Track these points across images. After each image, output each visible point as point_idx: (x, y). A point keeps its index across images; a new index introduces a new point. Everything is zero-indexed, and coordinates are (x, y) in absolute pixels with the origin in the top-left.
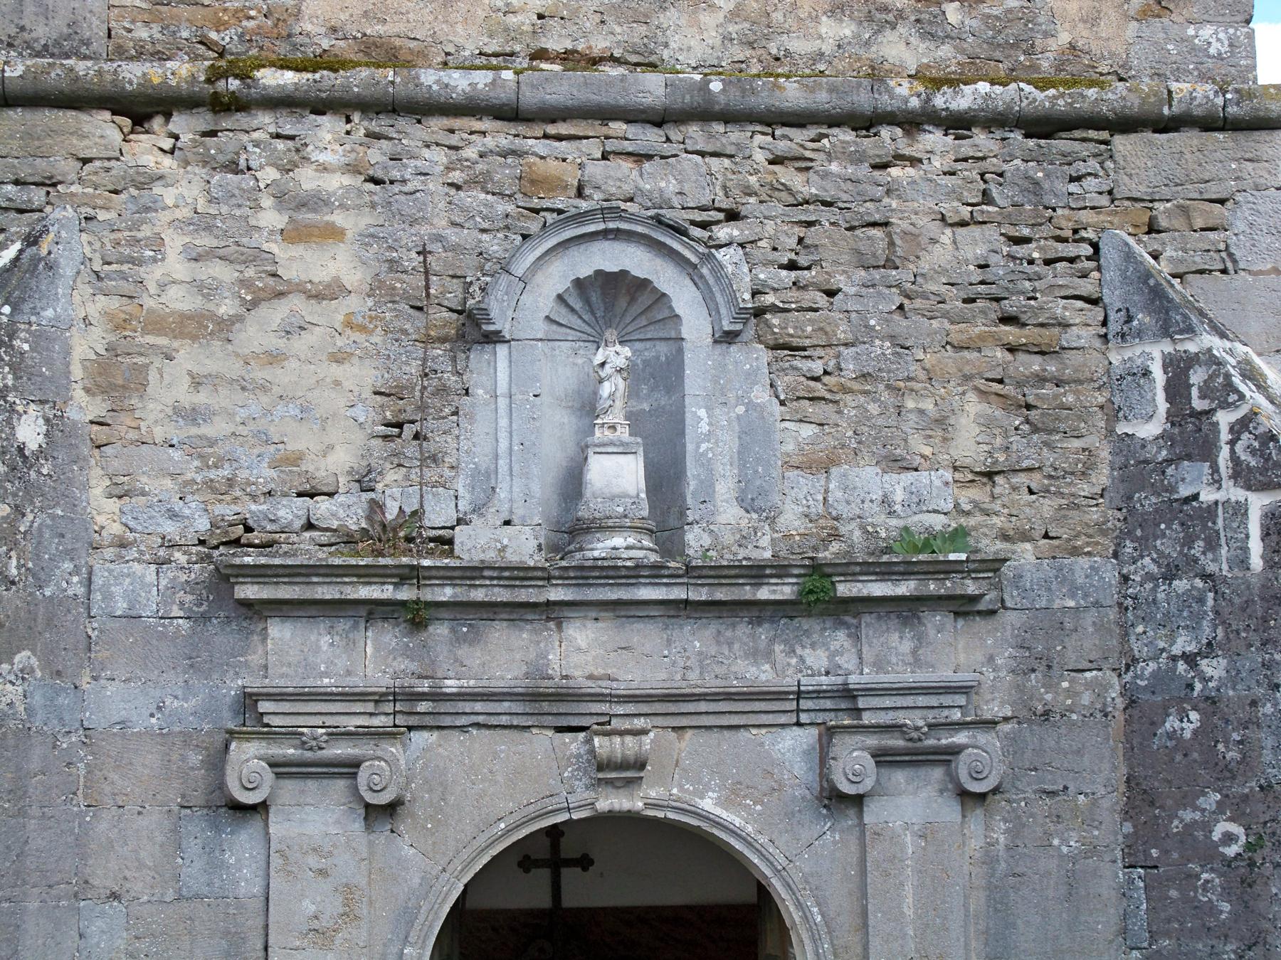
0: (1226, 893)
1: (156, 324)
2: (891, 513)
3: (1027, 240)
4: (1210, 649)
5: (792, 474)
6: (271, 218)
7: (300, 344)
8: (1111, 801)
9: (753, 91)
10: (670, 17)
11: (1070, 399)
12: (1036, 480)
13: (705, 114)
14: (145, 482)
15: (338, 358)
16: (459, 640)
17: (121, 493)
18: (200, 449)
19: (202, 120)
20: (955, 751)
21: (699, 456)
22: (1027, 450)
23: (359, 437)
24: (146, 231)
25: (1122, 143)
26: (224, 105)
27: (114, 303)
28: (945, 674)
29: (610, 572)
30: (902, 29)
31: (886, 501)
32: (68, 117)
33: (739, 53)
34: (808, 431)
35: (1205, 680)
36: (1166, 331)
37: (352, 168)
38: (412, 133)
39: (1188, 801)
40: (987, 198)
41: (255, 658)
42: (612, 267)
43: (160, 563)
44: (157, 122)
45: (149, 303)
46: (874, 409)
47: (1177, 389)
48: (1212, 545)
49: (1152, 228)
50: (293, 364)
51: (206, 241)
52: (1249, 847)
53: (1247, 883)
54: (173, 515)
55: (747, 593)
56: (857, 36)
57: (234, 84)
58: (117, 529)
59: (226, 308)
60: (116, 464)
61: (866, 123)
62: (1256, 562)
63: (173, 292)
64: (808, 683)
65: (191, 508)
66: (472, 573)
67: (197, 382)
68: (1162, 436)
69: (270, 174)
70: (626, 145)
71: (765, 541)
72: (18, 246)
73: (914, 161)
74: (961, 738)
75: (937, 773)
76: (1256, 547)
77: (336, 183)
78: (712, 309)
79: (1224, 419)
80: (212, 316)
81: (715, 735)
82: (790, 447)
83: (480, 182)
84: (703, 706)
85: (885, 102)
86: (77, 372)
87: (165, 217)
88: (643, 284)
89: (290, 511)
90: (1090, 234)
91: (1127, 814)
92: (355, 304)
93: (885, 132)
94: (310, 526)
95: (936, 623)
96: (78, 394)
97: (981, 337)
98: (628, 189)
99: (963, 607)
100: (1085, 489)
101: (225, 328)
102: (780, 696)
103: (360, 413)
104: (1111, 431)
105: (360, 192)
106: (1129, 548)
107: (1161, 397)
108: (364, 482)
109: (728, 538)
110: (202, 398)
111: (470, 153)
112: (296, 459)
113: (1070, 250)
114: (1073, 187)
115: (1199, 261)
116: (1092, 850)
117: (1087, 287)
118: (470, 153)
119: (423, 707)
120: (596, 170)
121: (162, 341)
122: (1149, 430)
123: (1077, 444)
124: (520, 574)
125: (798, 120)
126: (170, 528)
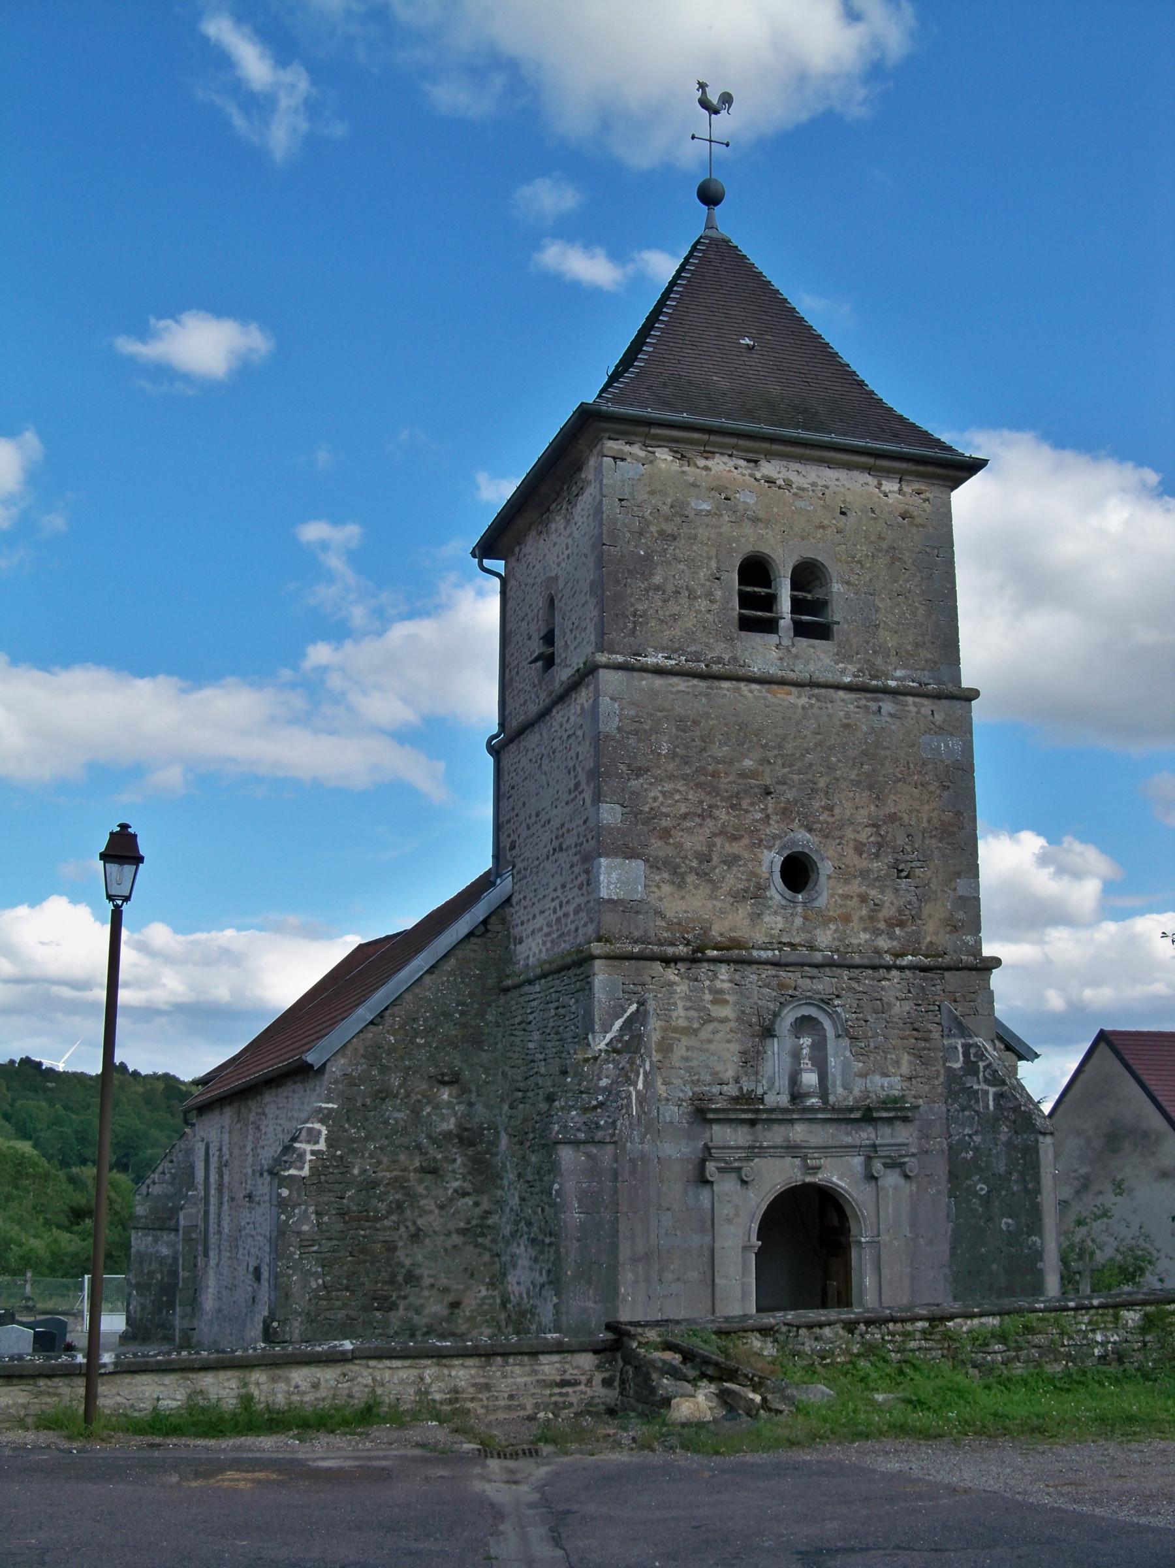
0: (981, 1206)
1: (675, 1030)
2: (884, 1090)
3: (920, 1005)
4: (976, 1133)
5: (857, 1078)
6: (708, 997)
7: (718, 1037)
8: (944, 1178)
9: (846, 959)
10: (817, 932)
11: (932, 1055)
12: (923, 1080)
13: (832, 964)
14: (674, 1081)
15: (729, 1041)
16: (764, 1130)
17: (665, 1083)
18: (689, 1070)
19: (687, 965)
20: (904, 1163)
21: (832, 1073)
22: (921, 1071)
23: (735, 1066)
24: (672, 1001)
25: (947, 974)
26: (694, 961)
27: (663, 1023)
28: (900, 1140)
29: (812, 1109)
30: (883, 936)
31: (882, 1086)
32: (648, 963)
33: (837, 943)
34: (861, 1065)
35: (974, 1142)
36: (963, 1036)
37: (731, 981)
38: (748, 970)
39: (969, 1178)
40: (909, 992)
41: (707, 1135)
42: (806, 1014)
43: (679, 1106)
44: (672, 965)
45: (673, 1023)
46: (879, 1058)
47: (966, 1054)
48: (977, 1101)
49: (955, 1001)
50: (715, 1043)
51: (688, 1004)
52: (988, 1192)
53: (988, 1202)
54: (682, 1091)
55: (847, 1116)
56: (871, 938)
57: (699, 955)
58: (665, 1095)
59: (696, 1025)
60: (664, 1075)
61: (874, 968)
62: (991, 1107)
63: (681, 1020)
64: (864, 1143)
65: (687, 1088)
66: (772, 1111)
67: (688, 1049)
68: (962, 1068)
69: (707, 983)
70: (809, 975)
71: (851, 1099)
72: (635, 1005)
73: (889, 980)
74: (906, 1159)
75: (898, 1170)
76: (991, 1103)
77: (727, 985)
78: (835, 1027)
79: (981, 1064)
80: (692, 1028)
81: (835, 1159)
82: (856, 1070)
83: (768, 986)
84: (834, 1150)
85: (883, 962)
86: (654, 1046)
87: (677, 996)
88: (815, 1019)
89: (716, 1089)
90: (937, 1003)
91: (949, 1181)
92: (733, 1024)
93: (881, 971)
94: (721, 1094)
95: (899, 1125)
96: (654, 1052)
97: (909, 1035)
98: (809, 988)
99: (905, 1119)
100: (937, 1083)
101: (695, 1032)
102: (855, 1147)
103: (735, 1059)
104: (944, 1064)
105: (733, 989)
106: (950, 1100)
107: (961, 1056)
108: (737, 1081)
109: (840, 1098)
110: (689, 1054)
111: (764, 976)
112: (717, 1073)
113: (931, 1007)
114: (933, 989)
115: (968, 1011)
116: (939, 1192)
117: (937, 1020)
118: (764, 976)
119: (756, 1150)
120: (800, 981)
121: (677, 1036)
122: (957, 1065)
123: (934, 1069)
124: (785, 1111)
125: (857, 967)
126: (681, 1095)
